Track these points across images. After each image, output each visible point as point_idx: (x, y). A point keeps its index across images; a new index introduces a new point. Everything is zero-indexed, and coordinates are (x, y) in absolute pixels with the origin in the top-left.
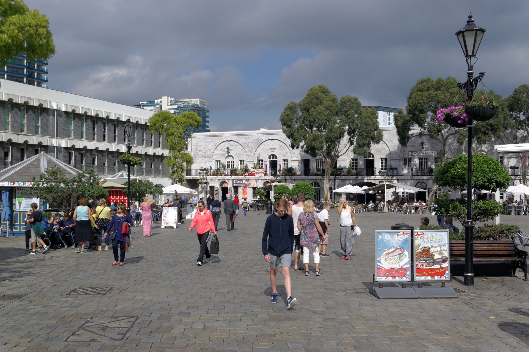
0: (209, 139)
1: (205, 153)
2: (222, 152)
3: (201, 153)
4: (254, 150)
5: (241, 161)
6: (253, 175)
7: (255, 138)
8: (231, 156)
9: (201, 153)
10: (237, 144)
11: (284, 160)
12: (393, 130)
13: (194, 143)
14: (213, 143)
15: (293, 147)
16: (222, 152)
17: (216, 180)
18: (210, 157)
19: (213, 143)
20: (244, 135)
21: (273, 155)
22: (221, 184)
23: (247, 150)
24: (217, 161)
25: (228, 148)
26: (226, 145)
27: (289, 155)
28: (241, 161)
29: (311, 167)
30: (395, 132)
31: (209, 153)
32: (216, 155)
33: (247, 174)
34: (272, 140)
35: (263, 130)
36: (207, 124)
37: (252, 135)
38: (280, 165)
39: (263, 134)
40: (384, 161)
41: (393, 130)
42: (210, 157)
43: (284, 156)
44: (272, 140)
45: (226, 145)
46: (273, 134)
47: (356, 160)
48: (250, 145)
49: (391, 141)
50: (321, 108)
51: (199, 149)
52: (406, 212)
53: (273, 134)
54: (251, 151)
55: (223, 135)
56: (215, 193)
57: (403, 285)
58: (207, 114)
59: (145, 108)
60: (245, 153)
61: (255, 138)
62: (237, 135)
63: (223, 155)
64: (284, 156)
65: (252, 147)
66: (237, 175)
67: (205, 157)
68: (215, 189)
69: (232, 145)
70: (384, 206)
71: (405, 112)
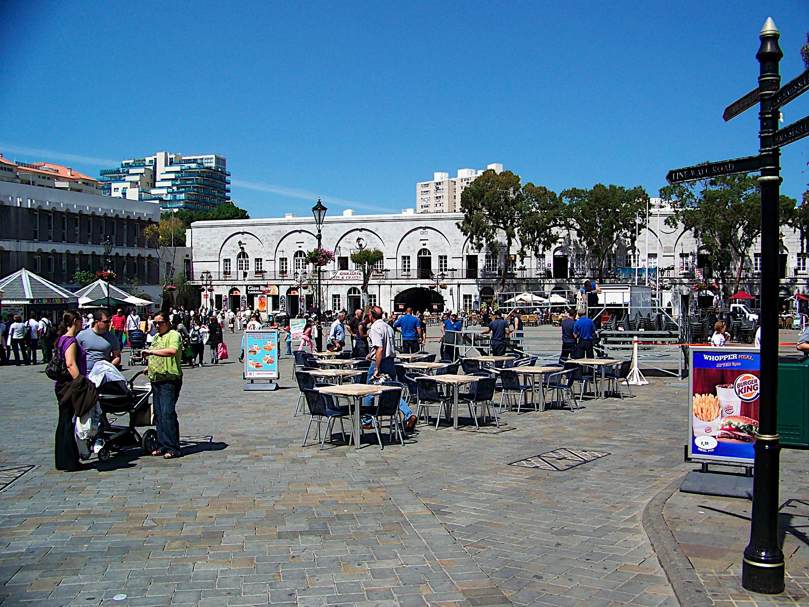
1: (209, 249)
23: (265, 244)
25: (240, 243)
63: (234, 251)
65: (273, 241)
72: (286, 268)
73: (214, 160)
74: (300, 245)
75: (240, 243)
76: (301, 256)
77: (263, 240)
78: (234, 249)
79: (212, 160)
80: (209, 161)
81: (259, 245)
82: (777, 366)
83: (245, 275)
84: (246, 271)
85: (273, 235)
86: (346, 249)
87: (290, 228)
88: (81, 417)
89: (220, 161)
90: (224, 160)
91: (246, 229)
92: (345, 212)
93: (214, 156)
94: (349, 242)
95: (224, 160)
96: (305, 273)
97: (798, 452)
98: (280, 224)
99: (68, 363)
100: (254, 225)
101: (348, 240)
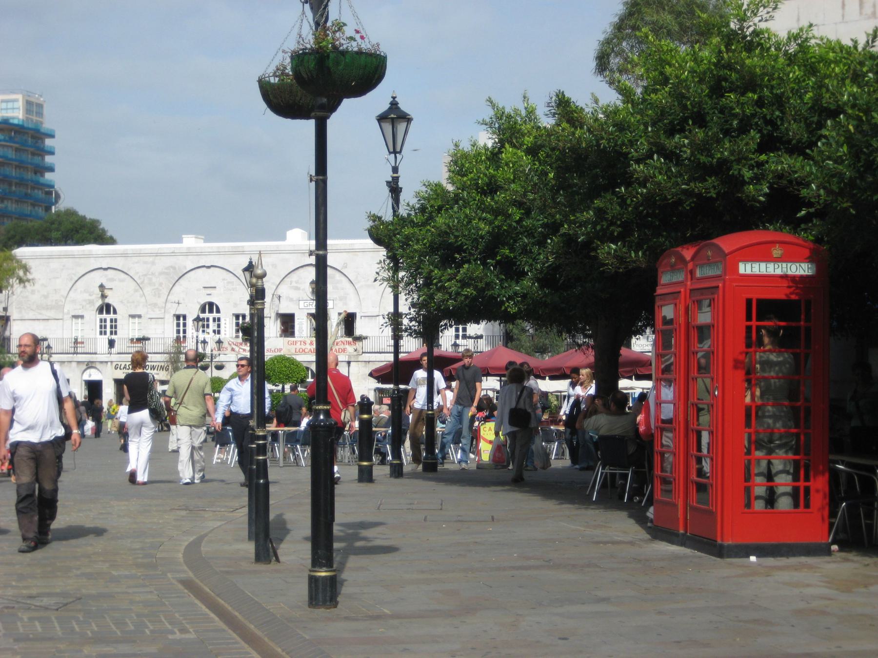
0: (55, 264)
1: (46, 297)
2: (86, 296)
4: (165, 292)
5: (178, 317)
7: (168, 261)
10: (123, 276)
16: (86, 296)
17: (74, 364)
18: (59, 307)
21: (211, 305)
23: (148, 290)
25: (102, 287)
28: (178, 317)
32: (74, 301)
34: (209, 267)
35: (190, 242)
36: (48, 159)
37: (157, 255)
39: (188, 253)
40: (181, 321)
42: (59, 307)
44: (209, 267)
46: (210, 254)
48: (154, 280)
53: (210, 254)
55: (89, 256)
58: (48, 142)
60: (143, 299)
61: (168, 261)
63: (91, 302)
65: (161, 284)
67: (48, 308)
69: (112, 280)
72: (184, 332)
73: (20, 104)
74: (209, 291)
75: (102, 287)
76: (211, 311)
77: (142, 282)
78: (90, 298)
79: (16, 105)
80: (10, 105)
81: (136, 291)
82: (619, 355)
83: (111, 343)
84: (113, 337)
85: (161, 273)
86: (291, 300)
87: (189, 264)
88: (221, 445)
89: (33, 107)
90: (40, 106)
91: (118, 263)
92: (289, 234)
93: (20, 97)
94: (297, 288)
95: (40, 106)
96: (219, 342)
97: (803, 566)
98: (173, 254)
99: (779, 272)
100: (125, 255)
101: (294, 284)
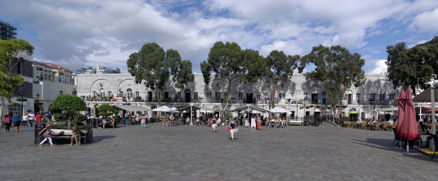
0: (88, 78)
1: (86, 86)
2: (97, 86)
3: (83, 86)
6: (116, 101)
7: (118, 78)
8: (103, 89)
9: (83, 86)
11: (137, 92)
12: (201, 75)
13: (79, 78)
14: (91, 80)
15: (137, 82)
16: (97, 86)
19: (91, 80)
20: (111, 76)
21: (130, 89)
22: (95, 106)
24: (94, 92)
26: (100, 81)
27: (140, 89)
29: (153, 97)
30: (203, 77)
31: (89, 86)
32: (93, 88)
33: (111, 100)
38: (134, 95)
41: (201, 75)
43: (136, 89)
45: (100, 81)
47: (180, 93)
49: (200, 82)
50: (152, 54)
51: (82, 84)
52: (188, 124)
54: (115, 86)
56: (91, 112)
57: (255, 109)
59: (87, 70)
61: (118, 78)
62: (107, 76)
63: (98, 88)
64: (136, 89)
66: (106, 101)
67: (86, 89)
68: (91, 109)
70: (190, 121)
71: (207, 62)
